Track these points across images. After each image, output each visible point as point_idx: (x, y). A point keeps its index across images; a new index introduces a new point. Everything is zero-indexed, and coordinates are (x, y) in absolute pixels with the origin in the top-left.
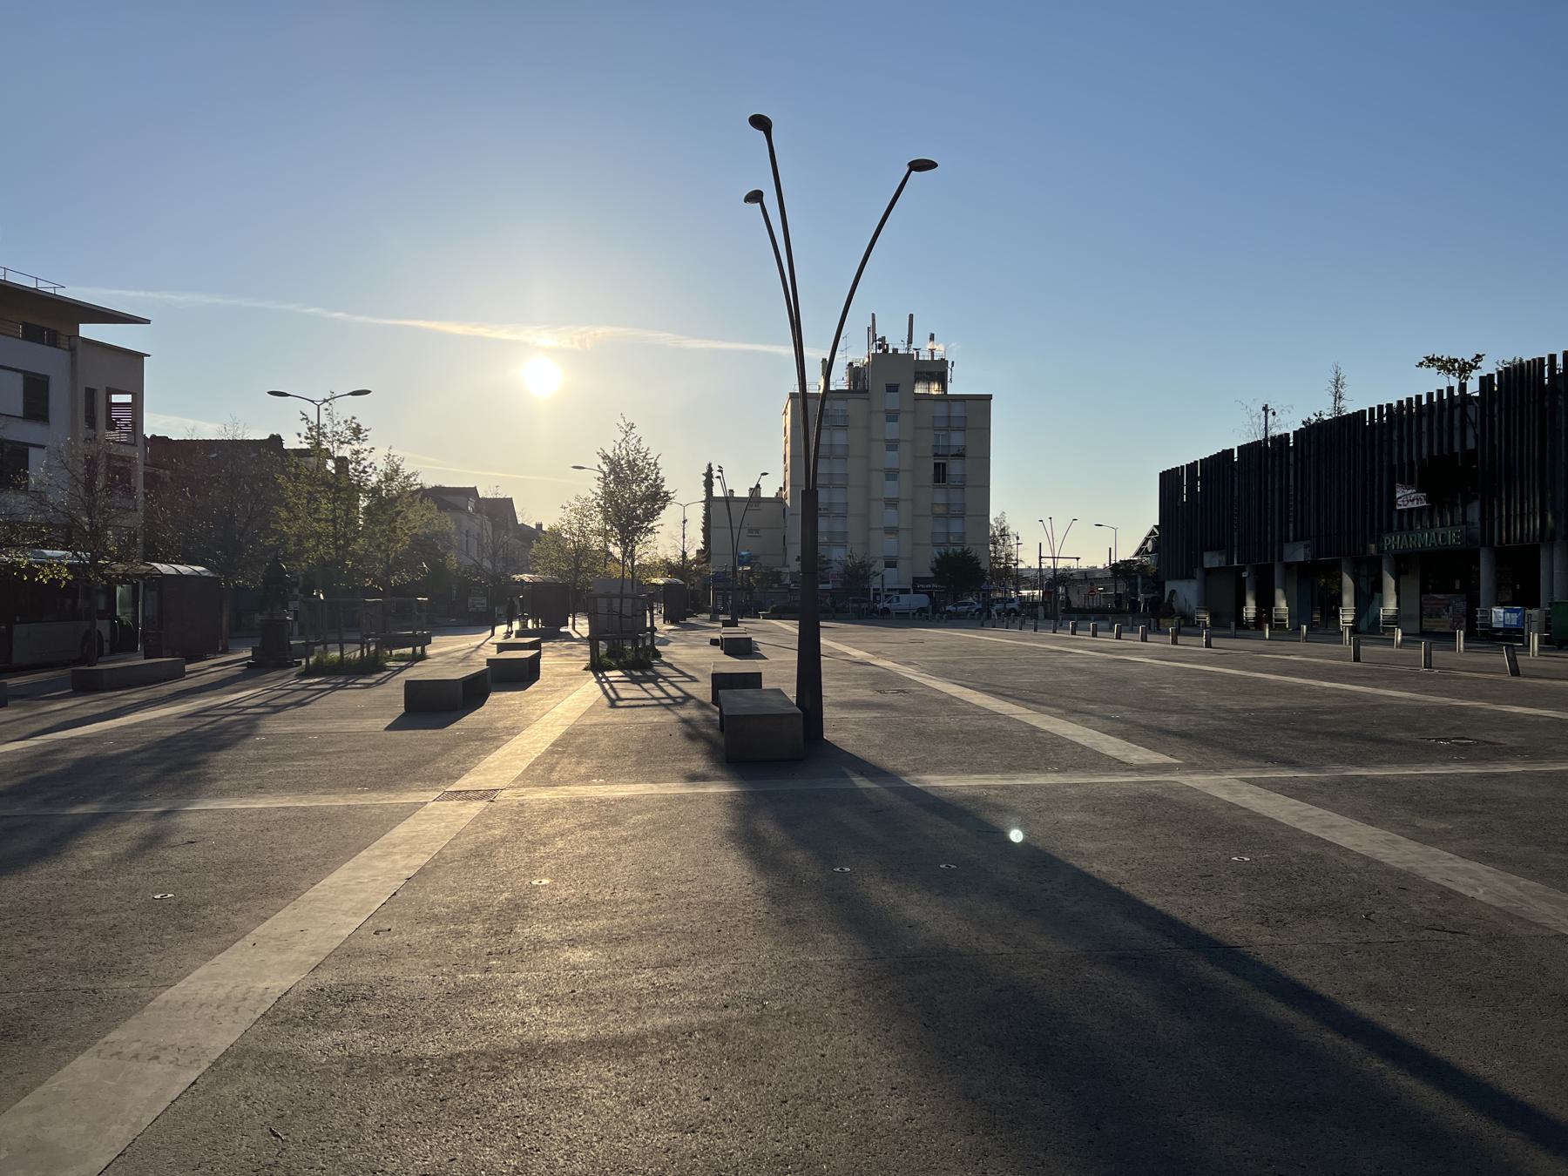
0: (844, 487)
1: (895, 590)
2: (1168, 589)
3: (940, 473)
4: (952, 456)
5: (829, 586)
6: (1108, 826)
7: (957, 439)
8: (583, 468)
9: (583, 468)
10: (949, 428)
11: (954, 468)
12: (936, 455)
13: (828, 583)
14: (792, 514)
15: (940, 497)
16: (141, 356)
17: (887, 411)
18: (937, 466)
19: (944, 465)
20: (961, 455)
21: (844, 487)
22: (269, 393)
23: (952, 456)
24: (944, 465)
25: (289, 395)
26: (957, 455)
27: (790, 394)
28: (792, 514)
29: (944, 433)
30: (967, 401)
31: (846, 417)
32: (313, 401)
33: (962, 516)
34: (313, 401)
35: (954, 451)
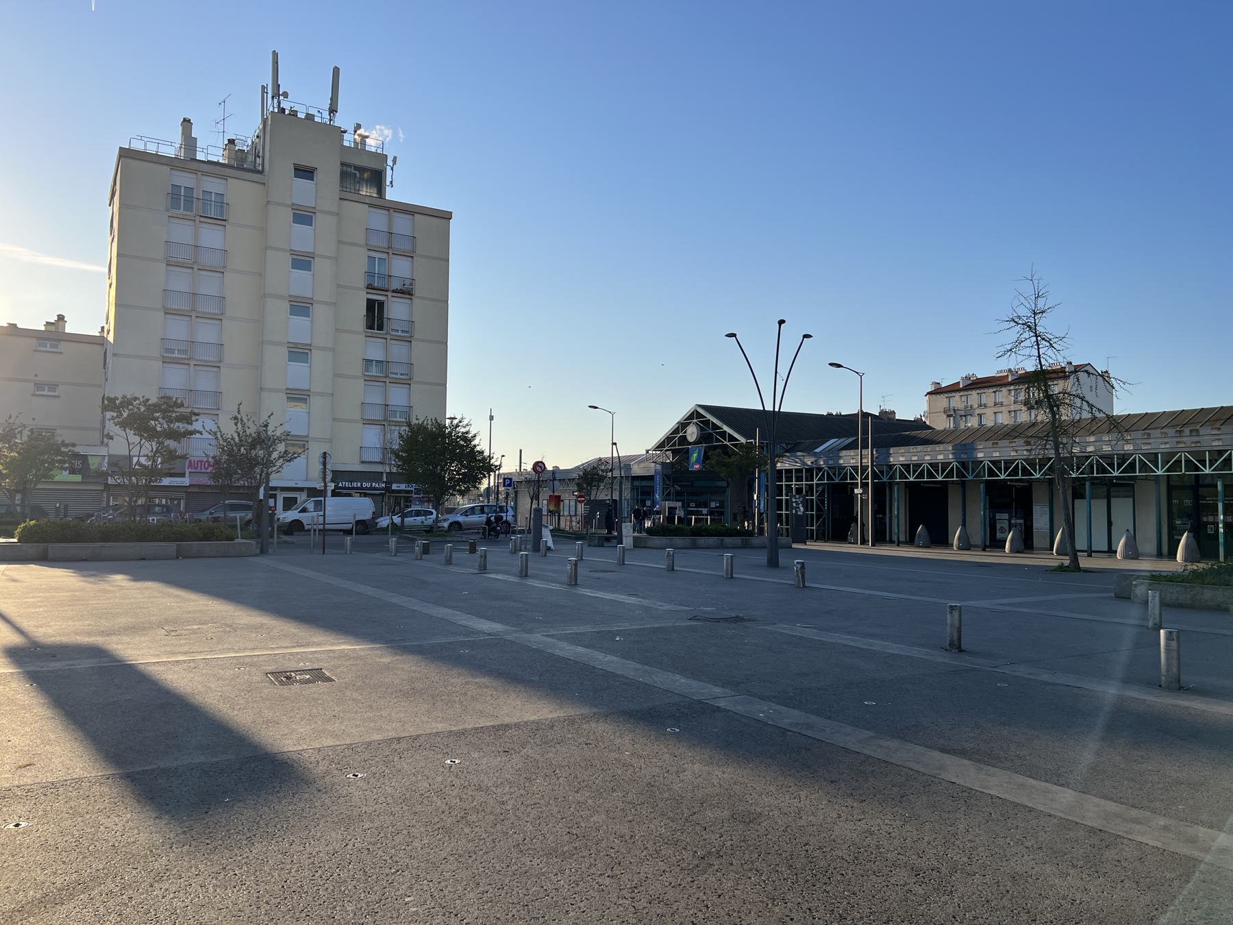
0: (218, 318)
1: (301, 489)
2: (127, 411)
3: (375, 316)
4: (394, 291)
5: (186, 481)
6: (622, 872)
7: (400, 269)
8: (597, 408)
9: (597, 408)
10: (389, 250)
11: (396, 309)
12: (370, 287)
13: (183, 475)
14: (114, 355)
15: (375, 350)
16: (446, 216)
17: (294, 207)
18: (371, 304)
19: (381, 304)
20: (406, 292)
21: (218, 318)
22: (726, 336)
23: (394, 291)
24: (381, 304)
25: (842, 367)
26: (402, 292)
27: (121, 148)
28: (114, 355)
29: (384, 256)
30: (416, 215)
31: (222, 204)
32: (857, 373)
33: (407, 382)
34: (857, 373)
35: (396, 285)
